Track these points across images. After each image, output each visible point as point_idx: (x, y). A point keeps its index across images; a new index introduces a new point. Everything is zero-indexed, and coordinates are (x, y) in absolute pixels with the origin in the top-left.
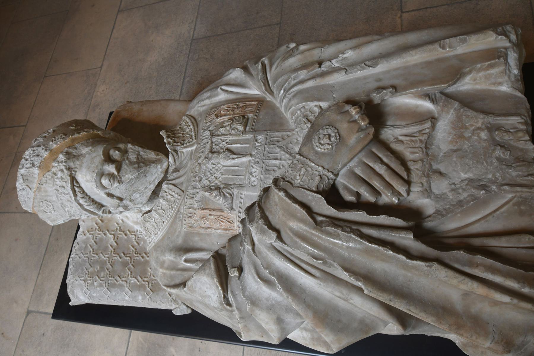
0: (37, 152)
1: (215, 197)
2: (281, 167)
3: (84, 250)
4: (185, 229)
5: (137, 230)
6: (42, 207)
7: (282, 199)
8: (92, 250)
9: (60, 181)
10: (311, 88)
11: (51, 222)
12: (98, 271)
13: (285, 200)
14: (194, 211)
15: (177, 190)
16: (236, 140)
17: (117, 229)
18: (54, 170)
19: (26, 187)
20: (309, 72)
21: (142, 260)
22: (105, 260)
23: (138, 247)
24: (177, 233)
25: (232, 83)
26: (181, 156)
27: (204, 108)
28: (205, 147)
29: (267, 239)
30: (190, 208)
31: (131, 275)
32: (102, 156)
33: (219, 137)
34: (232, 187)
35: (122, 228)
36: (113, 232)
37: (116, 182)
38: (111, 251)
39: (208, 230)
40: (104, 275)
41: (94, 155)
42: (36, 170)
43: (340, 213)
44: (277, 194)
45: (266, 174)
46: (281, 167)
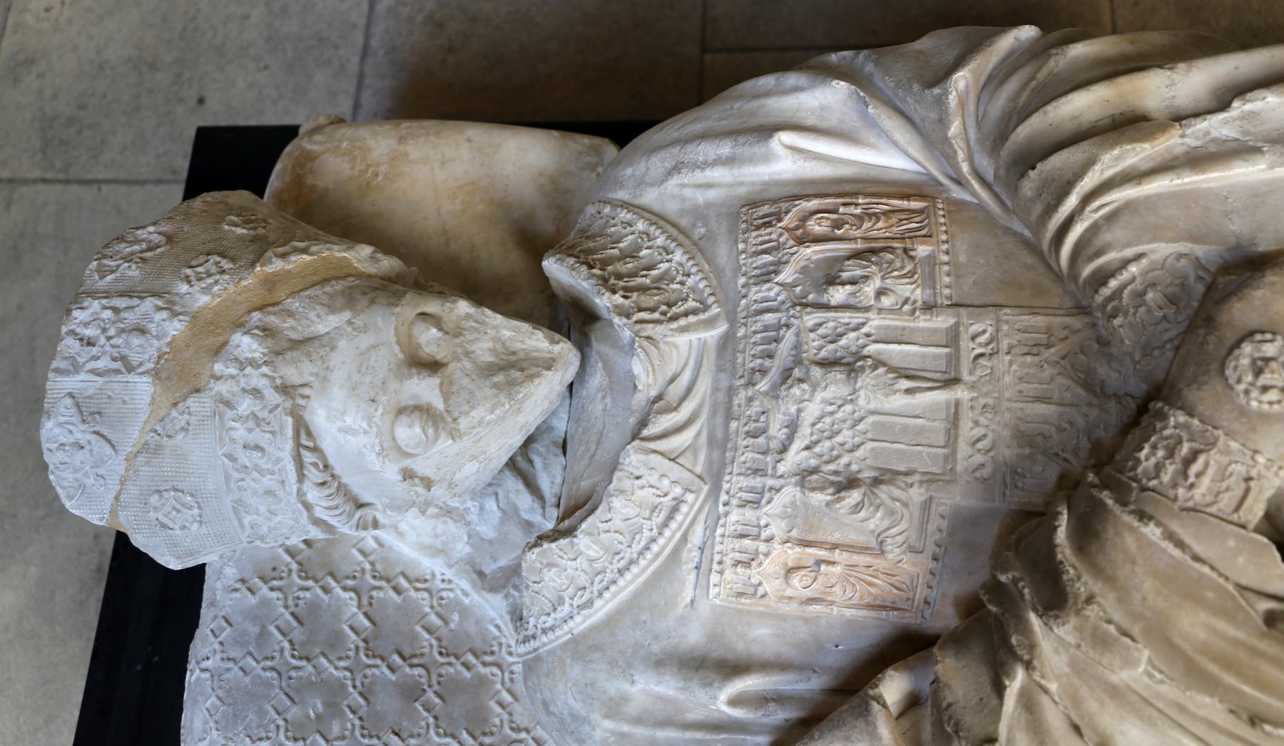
0: (131, 318)
1: (857, 508)
3: (259, 645)
5: (433, 575)
6: (156, 509)
7: (1151, 544)
8: (287, 645)
9: (250, 430)
11: (178, 558)
12: (318, 716)
13: (1164, 551)
16: (897, 328)
17: (363, 571)
18: (222, 388)
19: (93, 437)
21: (468, 675)
22: (338, 679)
23: (444, 632)
25: (810, 122)
27: (712, 194)
30: (743, 536)
31: (437, 727)
32: (397, 348)
33: (832, 314)
34: (909, 480)
35: (379, 567)
36: (350, 583)
37: (443, 436)
38: (357, 648)
39: (811, 608)
40: (344, 729)
41: (365, 340)
42: (143, 387)
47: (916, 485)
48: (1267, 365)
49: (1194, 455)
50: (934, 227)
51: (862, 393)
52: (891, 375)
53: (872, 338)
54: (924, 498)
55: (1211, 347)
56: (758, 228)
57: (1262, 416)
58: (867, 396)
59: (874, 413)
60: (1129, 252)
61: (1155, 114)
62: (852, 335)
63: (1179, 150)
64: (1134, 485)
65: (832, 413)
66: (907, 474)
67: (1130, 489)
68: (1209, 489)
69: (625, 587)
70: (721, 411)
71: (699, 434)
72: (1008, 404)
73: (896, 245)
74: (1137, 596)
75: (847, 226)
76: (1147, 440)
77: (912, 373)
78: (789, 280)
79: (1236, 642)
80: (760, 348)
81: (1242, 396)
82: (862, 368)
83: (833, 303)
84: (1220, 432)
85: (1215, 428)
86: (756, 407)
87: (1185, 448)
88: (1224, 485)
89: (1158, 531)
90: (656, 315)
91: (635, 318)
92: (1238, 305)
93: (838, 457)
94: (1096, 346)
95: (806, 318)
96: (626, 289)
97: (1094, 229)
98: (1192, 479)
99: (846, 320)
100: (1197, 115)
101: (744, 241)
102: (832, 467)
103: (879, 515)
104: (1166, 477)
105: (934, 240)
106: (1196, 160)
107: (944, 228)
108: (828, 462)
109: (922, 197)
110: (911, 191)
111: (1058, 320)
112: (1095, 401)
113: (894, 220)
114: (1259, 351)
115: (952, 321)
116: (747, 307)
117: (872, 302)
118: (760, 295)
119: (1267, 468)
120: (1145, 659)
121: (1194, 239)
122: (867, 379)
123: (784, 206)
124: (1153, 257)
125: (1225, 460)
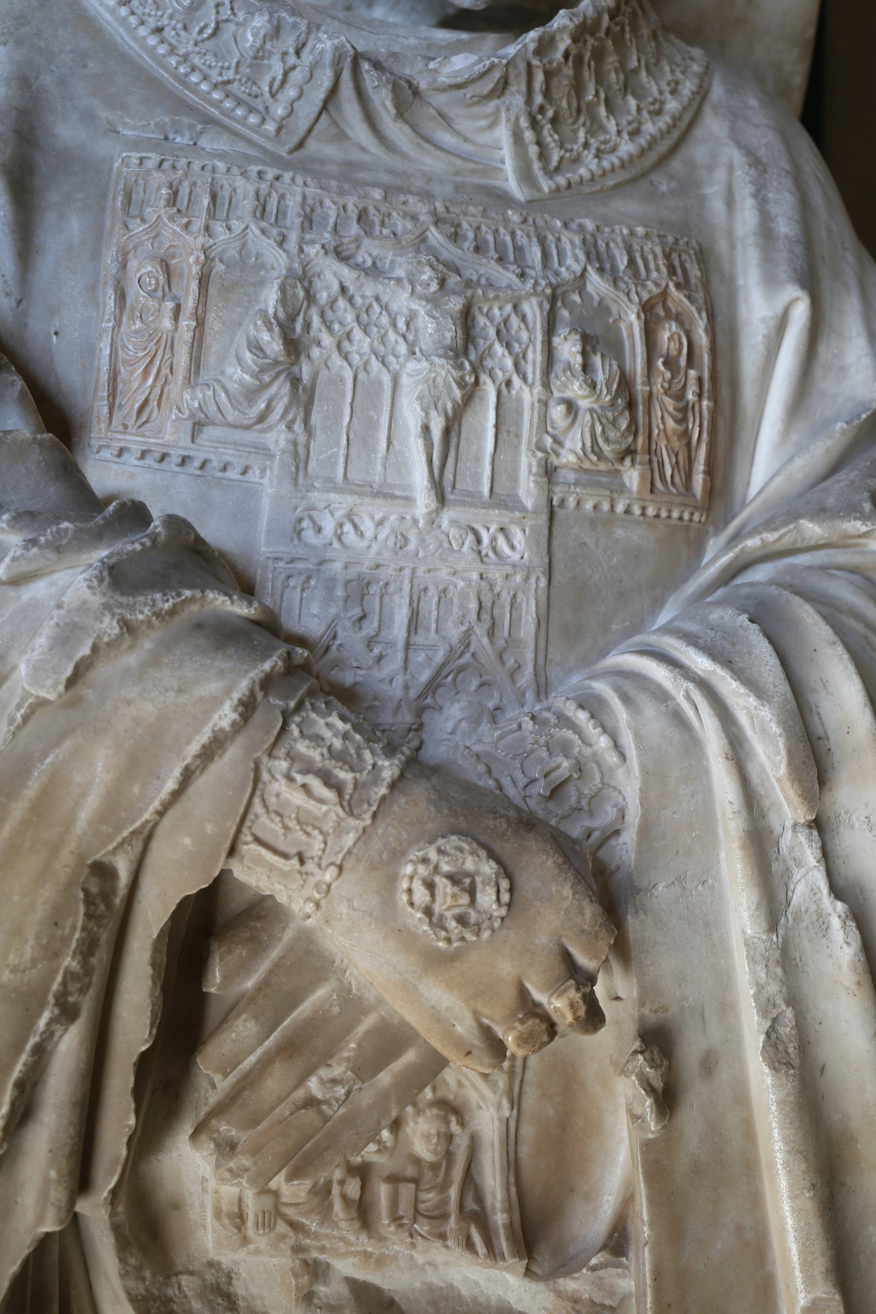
1: (256, 347)
2: (376, 651)
4: (124, 162)
7: (207, 714)
10: (708, 789)
13: (198, 730)
14: (198, 224)
15: (308, 110)
16: (519, 426)
20: (778, 780)
24: (103, 114)
25: (824, 351)
26: (476, 117)
27: (718, 205)
28: (501, 260)
29: (36, 655)
30: (214, 197)
33: (539, 337)
34: (298, 427)
39: (110, 292)
43: (147, 956)
44: (228, 691)
45: (348, 582)
46: (376, 651)
47: (290, 436)
48: (463, 890)
49: (337, 787)
50: (665, 498)
51: (425, 364)
52: (449, 406)
53: (504, 390)
54: (271, 446)
55: (491, 823)
56: (667, 256)
57: (392, 880)
58: (419, 372)
59: (396, 381)
60: (628, 740)
61: (827, 798)
62: (509, 363)
63: (774, 821)
64: (292, 704)
65: (394, 325)
66: (306, 421)
67: (287, 697)
68: (287, 803)
69: (135, 38)
70: (398, 181)
71: (363, 150)
72: (407, 572)
73: (640, 440)
74: (132, 692)
75: (668, 375)
76: (356, 728)
77: (454, 441)
78: (589, 288)
79: (71, 821)
80: (490, 238)
81: (420, 854)
82: (461, 367)
83: (556, 340)
84: (368, 822)
85: (374, 816)
86: (401, 224)
87: (345, 776)
88: (292, 824)
89: (225, 724)
90: (539, 99)
91: (535, 62)
92: (550, 862)
93: (329, 329)
94: (491, 705)
95: (534, 301)
96: (579, 61)
97: (662, 696)
98: (299, 778)
99: (530, 356)
100: (826, 855)
101: (647, 236)
102: (316, 321)
103: (247, 377)
104: (302, 747)
105: (647, 495)
106: (760, 842)
107: (664, 514)
108: (322, 315)
109: (710, 492)
110: (718, 482)
111: (530, 655)
112: (413, 693)
113: (676, 444)
114: (484, 883)
115: (529, 503)
116: (552, 230)
117: (556, 394)
118: (568, 247)
119: (317, 886)
120: (43, 694)
121: (645, 830)
122: (444, 370)
123: (700, 295)
124: (620, 773)
125: (328, 826)
